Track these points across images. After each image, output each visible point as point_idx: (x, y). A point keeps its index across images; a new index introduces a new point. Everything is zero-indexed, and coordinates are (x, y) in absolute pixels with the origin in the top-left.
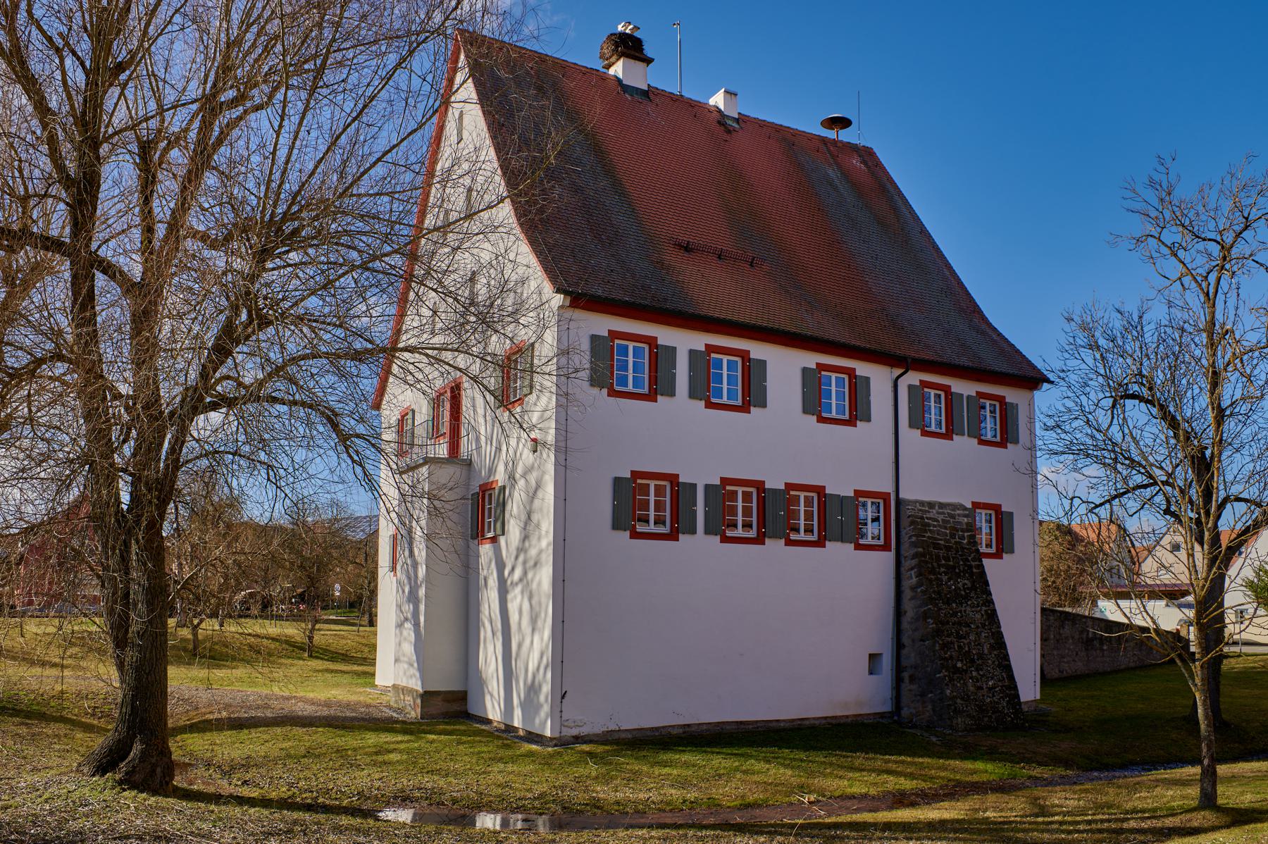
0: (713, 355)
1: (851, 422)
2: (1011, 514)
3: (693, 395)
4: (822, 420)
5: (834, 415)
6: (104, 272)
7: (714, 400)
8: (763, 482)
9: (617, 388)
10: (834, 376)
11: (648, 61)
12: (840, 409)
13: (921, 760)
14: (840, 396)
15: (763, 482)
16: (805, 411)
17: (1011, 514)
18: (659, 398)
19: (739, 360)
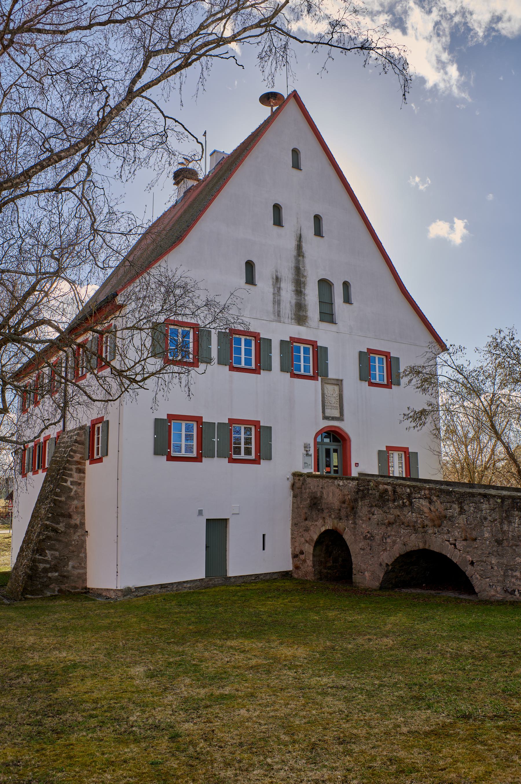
0: (295, 344)
1: (388, 386)
2: (398, 359)
3: (282, 370)
4: (371, 384)
5: (377, 381)
6: (143, 91)
7: (296, 372)
8: (259, 334)
9: (235, 365)
10: (377, 357)
11: (323, 237)
12: (381, 378)
13: (413, 591)
14: (381, 369)
15: (259, 334)
16: (361, 379)
17: (398, 359)
18: (262, 371)
19: (311, 347)
